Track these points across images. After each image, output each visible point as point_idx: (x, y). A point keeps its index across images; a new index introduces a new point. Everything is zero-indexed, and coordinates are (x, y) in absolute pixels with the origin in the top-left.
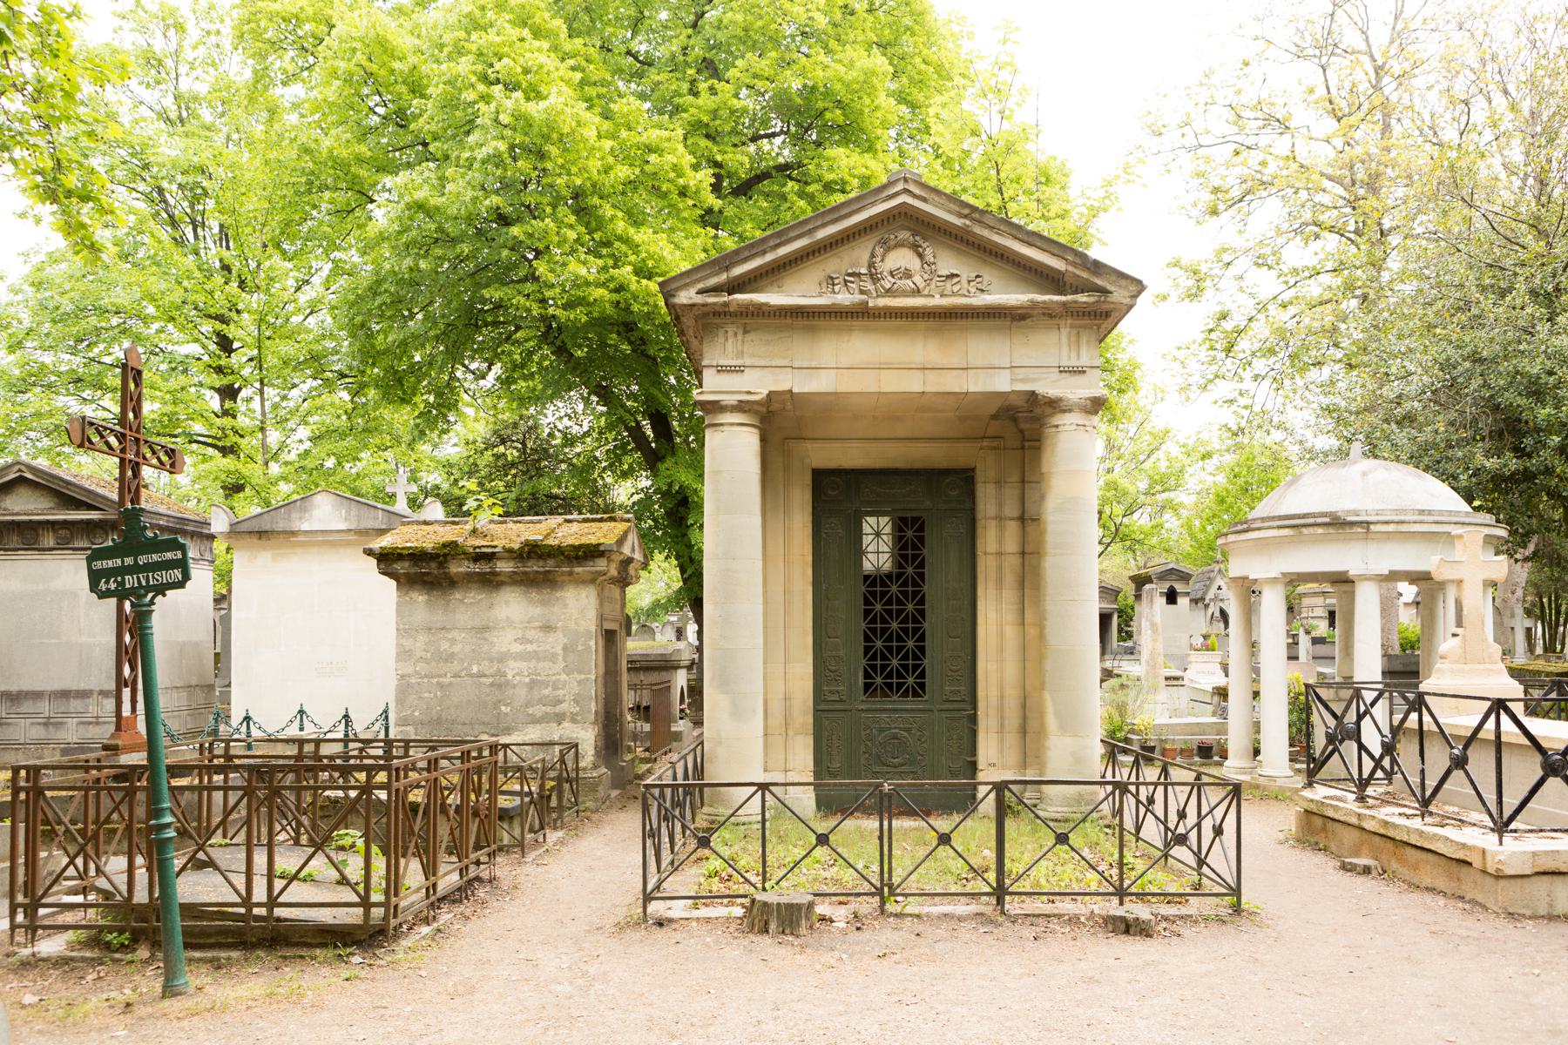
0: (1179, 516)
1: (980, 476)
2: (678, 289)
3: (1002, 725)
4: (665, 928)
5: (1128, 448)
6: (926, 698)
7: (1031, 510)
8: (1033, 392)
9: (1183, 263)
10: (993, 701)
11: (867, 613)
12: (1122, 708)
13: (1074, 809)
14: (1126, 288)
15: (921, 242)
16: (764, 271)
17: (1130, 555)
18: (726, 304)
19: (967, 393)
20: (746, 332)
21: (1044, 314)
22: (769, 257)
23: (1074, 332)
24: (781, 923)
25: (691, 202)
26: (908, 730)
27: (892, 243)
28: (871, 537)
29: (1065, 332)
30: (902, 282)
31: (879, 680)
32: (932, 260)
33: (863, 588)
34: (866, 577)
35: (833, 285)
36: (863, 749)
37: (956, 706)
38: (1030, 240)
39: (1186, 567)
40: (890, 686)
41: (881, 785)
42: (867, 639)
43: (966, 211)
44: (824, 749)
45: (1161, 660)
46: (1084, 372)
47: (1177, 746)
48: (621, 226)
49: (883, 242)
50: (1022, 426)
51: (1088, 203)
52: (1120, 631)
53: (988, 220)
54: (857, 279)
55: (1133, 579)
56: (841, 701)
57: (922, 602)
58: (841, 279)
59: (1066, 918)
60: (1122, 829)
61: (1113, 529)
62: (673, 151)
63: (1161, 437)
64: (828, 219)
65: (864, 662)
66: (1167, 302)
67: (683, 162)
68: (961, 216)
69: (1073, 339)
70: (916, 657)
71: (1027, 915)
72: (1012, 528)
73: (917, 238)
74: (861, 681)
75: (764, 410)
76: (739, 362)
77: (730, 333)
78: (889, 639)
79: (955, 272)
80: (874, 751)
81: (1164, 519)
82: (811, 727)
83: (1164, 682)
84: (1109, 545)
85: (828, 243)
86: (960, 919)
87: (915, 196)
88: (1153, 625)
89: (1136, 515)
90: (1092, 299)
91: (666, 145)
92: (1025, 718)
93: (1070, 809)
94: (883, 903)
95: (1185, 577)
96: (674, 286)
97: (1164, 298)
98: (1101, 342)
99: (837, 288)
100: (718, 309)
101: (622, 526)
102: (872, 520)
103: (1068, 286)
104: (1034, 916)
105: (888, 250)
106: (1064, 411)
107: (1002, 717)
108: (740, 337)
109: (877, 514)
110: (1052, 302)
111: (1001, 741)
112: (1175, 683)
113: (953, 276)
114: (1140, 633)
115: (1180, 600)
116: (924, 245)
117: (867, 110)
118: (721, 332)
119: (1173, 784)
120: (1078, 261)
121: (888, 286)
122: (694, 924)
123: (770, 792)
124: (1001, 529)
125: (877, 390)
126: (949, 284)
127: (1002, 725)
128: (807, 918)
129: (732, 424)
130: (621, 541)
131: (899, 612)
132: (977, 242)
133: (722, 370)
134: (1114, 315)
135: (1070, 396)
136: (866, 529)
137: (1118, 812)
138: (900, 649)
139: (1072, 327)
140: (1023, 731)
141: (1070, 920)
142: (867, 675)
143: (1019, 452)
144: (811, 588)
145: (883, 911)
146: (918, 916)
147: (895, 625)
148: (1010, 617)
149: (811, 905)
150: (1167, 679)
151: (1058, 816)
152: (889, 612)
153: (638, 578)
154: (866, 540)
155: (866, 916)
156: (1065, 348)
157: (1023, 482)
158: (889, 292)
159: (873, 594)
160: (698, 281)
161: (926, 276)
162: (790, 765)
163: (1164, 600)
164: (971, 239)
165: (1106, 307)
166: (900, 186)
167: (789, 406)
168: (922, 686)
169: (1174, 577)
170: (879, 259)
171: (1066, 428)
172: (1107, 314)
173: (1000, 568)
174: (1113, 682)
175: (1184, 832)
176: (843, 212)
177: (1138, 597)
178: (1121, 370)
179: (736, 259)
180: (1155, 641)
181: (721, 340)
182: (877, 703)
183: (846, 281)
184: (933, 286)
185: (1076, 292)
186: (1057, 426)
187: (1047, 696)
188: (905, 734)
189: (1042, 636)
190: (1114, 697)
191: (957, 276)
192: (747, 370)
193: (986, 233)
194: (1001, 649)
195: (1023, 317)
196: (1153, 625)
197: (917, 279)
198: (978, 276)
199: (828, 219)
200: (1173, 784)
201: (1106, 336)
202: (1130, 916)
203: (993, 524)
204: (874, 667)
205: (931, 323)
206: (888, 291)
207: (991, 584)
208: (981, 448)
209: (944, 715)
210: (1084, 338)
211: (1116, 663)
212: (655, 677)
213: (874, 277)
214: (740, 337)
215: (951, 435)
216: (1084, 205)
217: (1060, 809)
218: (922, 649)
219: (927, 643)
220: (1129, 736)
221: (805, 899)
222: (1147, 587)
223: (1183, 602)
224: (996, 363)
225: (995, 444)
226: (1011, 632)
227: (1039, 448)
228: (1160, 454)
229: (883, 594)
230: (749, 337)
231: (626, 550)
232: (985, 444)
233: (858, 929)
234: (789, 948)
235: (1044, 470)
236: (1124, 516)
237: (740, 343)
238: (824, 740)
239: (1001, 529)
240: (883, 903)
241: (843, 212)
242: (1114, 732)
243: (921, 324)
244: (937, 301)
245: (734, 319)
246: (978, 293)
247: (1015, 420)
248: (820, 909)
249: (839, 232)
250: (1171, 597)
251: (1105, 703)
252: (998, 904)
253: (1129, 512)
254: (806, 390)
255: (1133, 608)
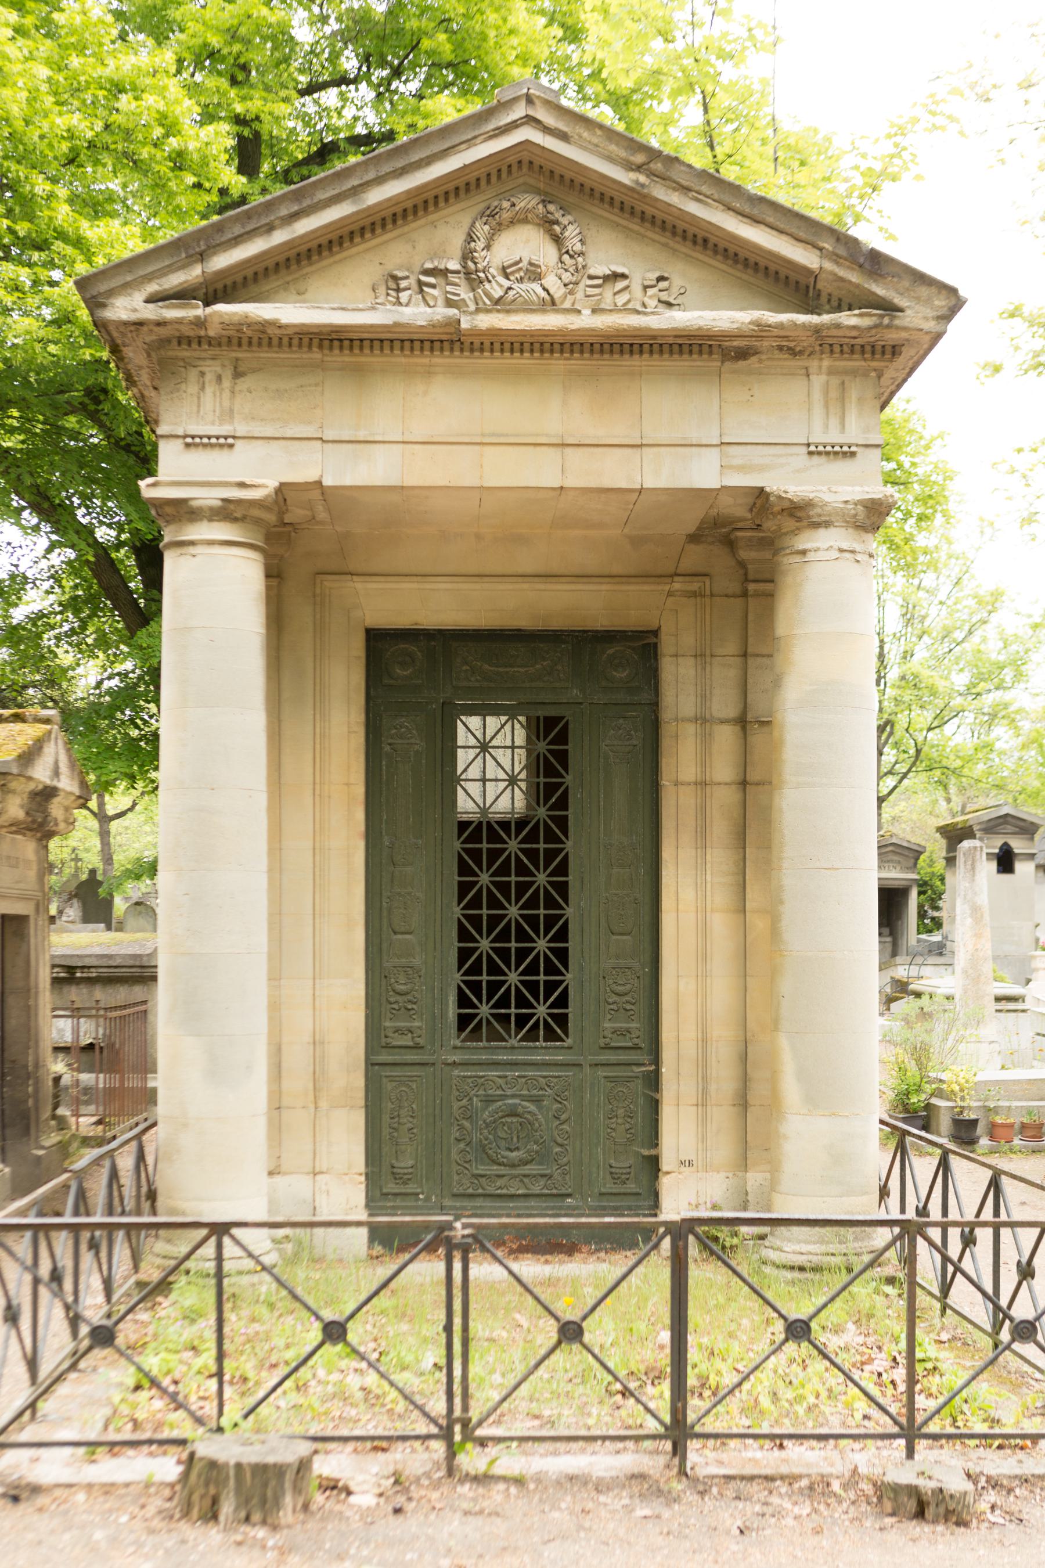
0: (1017, 732)
1: (667, 645)
2: (111, 293)
3: (705, 1092)
4: (22, 1507)
5: (936, 618)
6: (569, 1042)
7: (757, 708)
8: (761, 491)
9: (1026, 311)
10: (690, 1049)
11: (464, 889)
12: (921, 1054)
13: (831, 1248)
14: (928, 301)
15: (558, 215)
16: (270, 262)
17: (940, 794)
18: (200, 323)
19: (641, 491)
20: (238, 374)
21: (780, 348)
22: (280, 237)
23: (835, 381)
24: (244, 1501)
25: (191, 179)
26: (537, 1100)
27: (506, 216)
28: (472, 753)
29: (818, 381)
30: (523, 286)
31: (484, 1010)
32: (578, 247)
33: (458, 845)
34: (463, 825)
35: (398, 290)
36: (455, 1134)
37: (623, 1057)
38: (755, 212)
39: (1029, 811)
40: (504, 1019)
41: (449, 1226)
42: (463, 935)
43: (639, 158)
44: (386, 1131)
45: (988, 968)
46: (853, 454)
47: (1015, 1119)
48: (63, 213)
49: (490, 214)
50: (744, 554)
51: (864, 165)
52: (922, 915)
53: (678, 175)
54: (441, 281)
55: (943, 830)
56: (417, 1047)
57: (563, 869)
58: (412, 281)
59: (804, 1483)
60: (912, 1283)
61: (912, 752)
62: (162, 91)
63: (992, 602)
64: (386, 168)
65: (457, 977)
66: (1002, 373)
67: (178, 110)
68: (630, 167)
69: (834, 394)
70: (551, 969)
71: (729, 1478)
72: (726, 737)
73: (551, 207)
74: (452, 1011)
75: (271, 518)
76: (225, 429)
77: (209, 377)
78: (504, 936)
79: (620, 270)
80: (475, 1137)
81: (993, 735)
82: (361, 1094)
83: (994, 1006)
84: (905, 775)
85: (388, 213)
86: (601, 1487)
87: (547, 130)
88: (975, 910)
89: (949, 728)
90: (866, 322)
91: (148, 81)
92: (745, 1080)
93: (823, 1248)
94: (451, 1454)
95: (1028, 829)
96: (103, 287)
97: (997, 369)
98: (883, 407)
99: (404, 296)
100: (187, 331)
101: (36, 730)
102: (474, 722)
103: (824, 299)
104: (743, 1478)
105: (498, 228)
106: (816, 525)
107: (705, 1079)
108: (227, 383)
109: (483, 711)
110: (795, 324)
111: (703, 1120)
112: (1012, 1006)
113: (616, 276)
114: (953, 919)
115: (1019, 866)
116: (564, 221)
117: (492, 34)
118: (193, 374)
119: (1012, 1225)
120: (842, 251)
121: (497, 293)
122: (81, 1497)
123: (233, 1237)
124: (705, 741)
125: (476, 483)
126: (608, 292)
127: (705, 1092)
128: (297, 1490)
129: (211, 543)
130: (29, 756)
131: (522, 888)
132: (660, 215)
133: (192, 443)
134: (907, 353)
135: (827, 497)
136: (462, 737)
137: (910, 1261)
138: (522, 954)
139: (831, 372)
140: (743, 1103)
141: (811, 1488)
142: (463, 1001)
143: (739, 601)
144: (361, 845)
145: (450, 1471)
146: (519, 1481)
147: (513, 911)
148: (720, 896)
149: (304, 1466)
150: (998, 999)
151: (800, 1260)
152: (504, 888)
153: (71, 823)
154: (463, 757)
155: (417, 1480)
156: (818, 411)
157: (745, 655)
158: (499, 304)
159: (476, 855)
160: (149, 278)
161: (567, 277)
162: (322, 1164)
163: (993, 865)
164: (650, 211)
165: (892, 337)
166: (519, 111)
167: (322, 515)
168: (562, 1021)
169: (1010, 828)
170: (480, 245)
171: (821, 555)
172: (895, 350)
173: (702, 811)
174: (904, 1006)
175: (1030, 1316)
176: (415, 157)
177: (951, 861)
178: (921, 482)
179: (219, 239)
180: (978, 936)
181: (193, 388)
182: (481, 1051)
183: (421, 284)
184: (580, 295)
185: (839, 309)
186: (804, 552)
187: (783, 1042)
188: (532, 1107)
189: (775, 932)
190: (908, 1034)
191: (624, 276)
192: (239, 444)
193: (675, 199)
194: (703, 957)
195: (743, 354)
196: (975, 910)
197: (551, 281)
198: (661, 279)
199: (386, 168)
200: (1012, 1225)
201: (892, 394)
202: (927, 1485)
203: (690, 730)
204: (475, 987)
205: (576, 363)
206: (498, 301)
207: (687, 838)
208: (670, 594)
209: (601, 1072)
210: (853, 394)
211: (914, 971)
212: (121, 994)
213: (473, 278)
214: (227, 383)
215: (616, 569)
216: (856, 168)
217: (804, 1248)
218: (563, 955)
219: (570, 945)
220: (934, 1101)
221: (290, 1454)
222: (966, 844)
223: (1024, 869)
224: (694, 437)
225: (695, 586)
226: (721, 924)
227: (771, 595)
228: (989, 630)
229: (494, 855)
230: (244, 384)
231: (41, 773)
232: (676, 586)
233: (397, 1511)
234: (256, 1553)
235: (781, 630)
236: (930, 729)
237: (226, 394)
238: (386, 1118)
239: (705, 741)
240: (451, 1454)
241: (415, 157)
242: (907, 1094)
243: (559, 364)
244: (586, 321)
245: (216, 351)
246: (661, 308)
247: (730, 543)
248: (325, 1466)
249: (409, 193)
250: (1005, 861)
251: (887, 1040)
252: (675, 1452)
253: (939, 722)
254: (348, 482)
255: (942, 879)
